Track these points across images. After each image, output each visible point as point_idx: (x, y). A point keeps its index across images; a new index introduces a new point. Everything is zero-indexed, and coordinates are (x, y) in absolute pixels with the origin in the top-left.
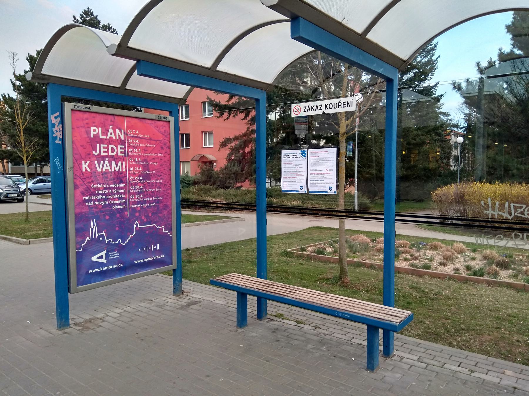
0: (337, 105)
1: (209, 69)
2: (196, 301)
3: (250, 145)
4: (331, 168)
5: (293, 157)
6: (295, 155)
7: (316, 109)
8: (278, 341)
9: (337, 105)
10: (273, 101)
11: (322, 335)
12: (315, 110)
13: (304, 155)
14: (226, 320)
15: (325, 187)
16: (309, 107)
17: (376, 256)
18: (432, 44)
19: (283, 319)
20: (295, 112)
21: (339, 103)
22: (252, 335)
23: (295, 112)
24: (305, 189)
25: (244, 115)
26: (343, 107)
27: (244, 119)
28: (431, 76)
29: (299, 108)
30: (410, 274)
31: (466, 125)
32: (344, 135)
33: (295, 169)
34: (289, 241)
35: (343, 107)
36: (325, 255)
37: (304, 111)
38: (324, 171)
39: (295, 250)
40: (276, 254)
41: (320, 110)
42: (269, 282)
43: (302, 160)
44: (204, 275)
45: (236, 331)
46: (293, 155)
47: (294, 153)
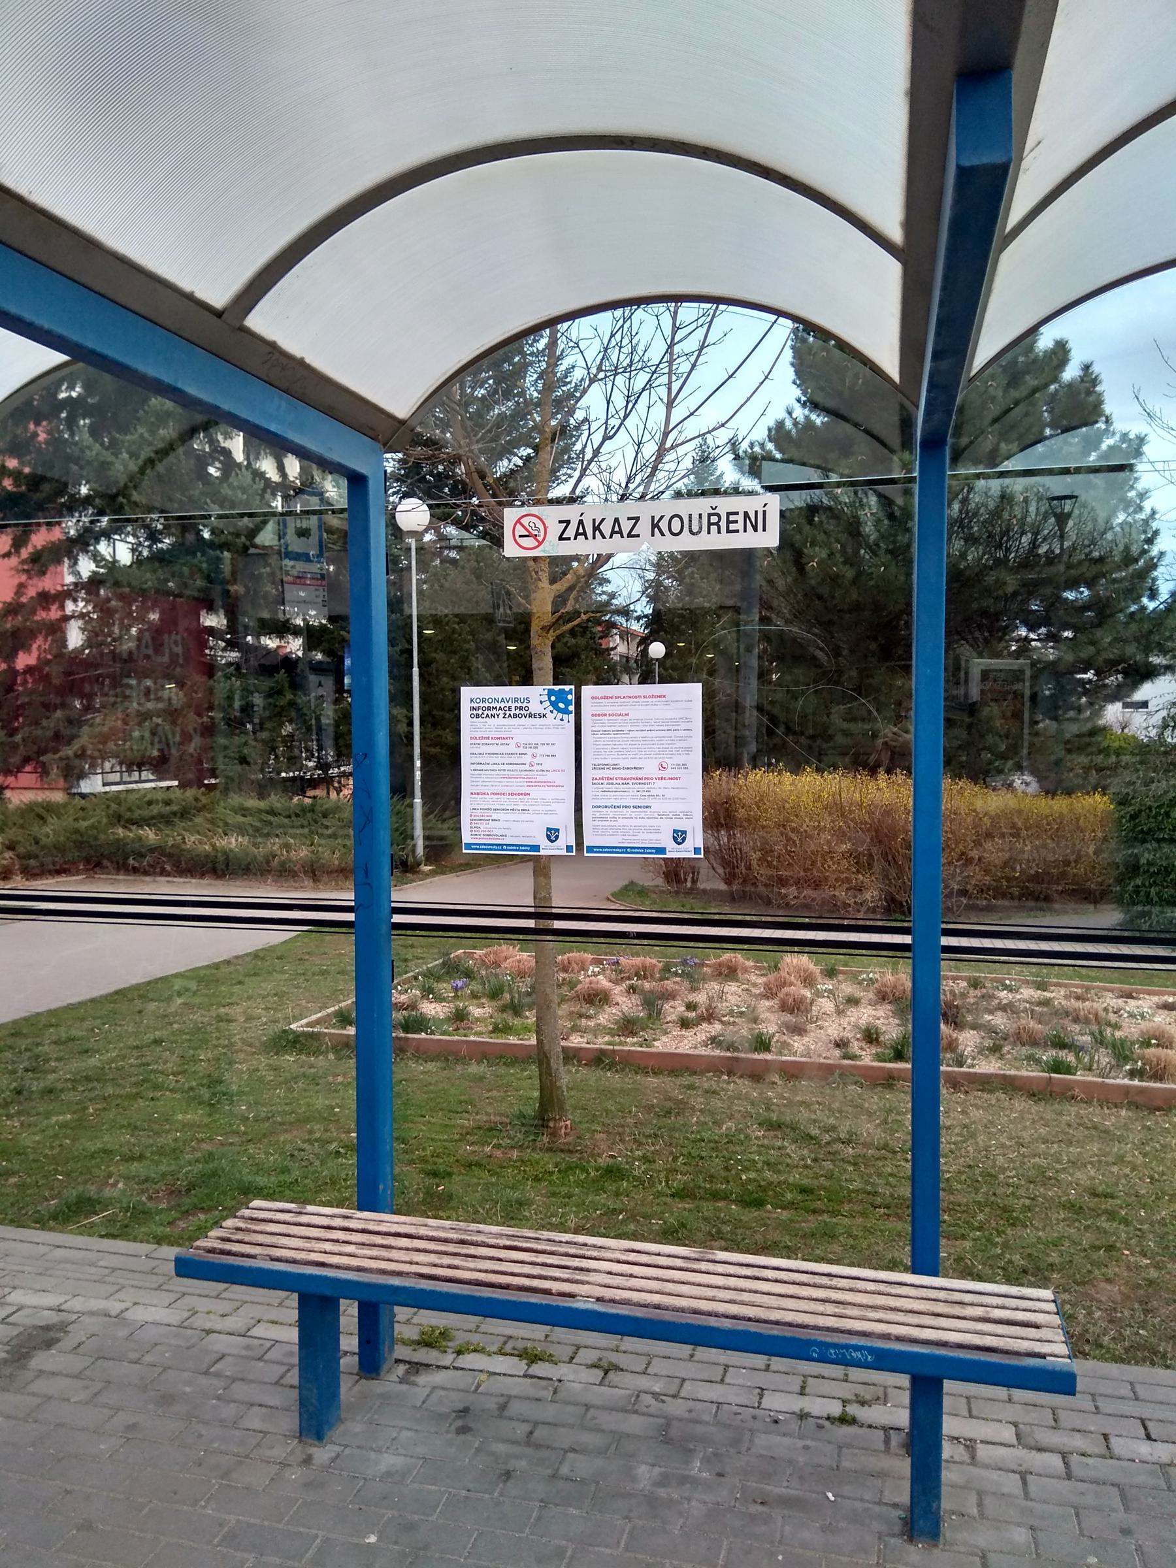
0: (700, 522)
1: (219, 314)
2: (47, 1328)
3: (35, 646)
4: (678, 759)
5: (515, 716)
6: (521, 708)
7: (613, 532)
8: (508, 1475)
9: (700, 522)
10: (124, 501)
11: (647, 1399)
12: (607, 534)
13: (562, 705)
14: (228, 1411)
15: (658, 831)
16: (581, 522)
17: (589, 1017)
18: (570, 382)
19: (459, 1353)
20: (520, 540)
21: (709, 515)
22: (383, 1468)
23: (520, 540)
24: (567, 837)
25: (10, 542)
26: (728, 531)
27: (7, 555)
28: (569, 472)
29: (539, 525)
30: (722, 1073)
31: (649, 610)
32: (548, 632)
33: (527, 759)
34: (268, 987)
35: (728, 531)
36: (432, 1033)
37: (561, 538)
38: (650, 768)
39: (318, 1022)
40: (250, 1045)
41: (630, 535)
42: (438, 1228)
43: (556, 727)
44: (13, 1180)
45: (308, 1461)
46: (513, 705)
47: (516, 700)
